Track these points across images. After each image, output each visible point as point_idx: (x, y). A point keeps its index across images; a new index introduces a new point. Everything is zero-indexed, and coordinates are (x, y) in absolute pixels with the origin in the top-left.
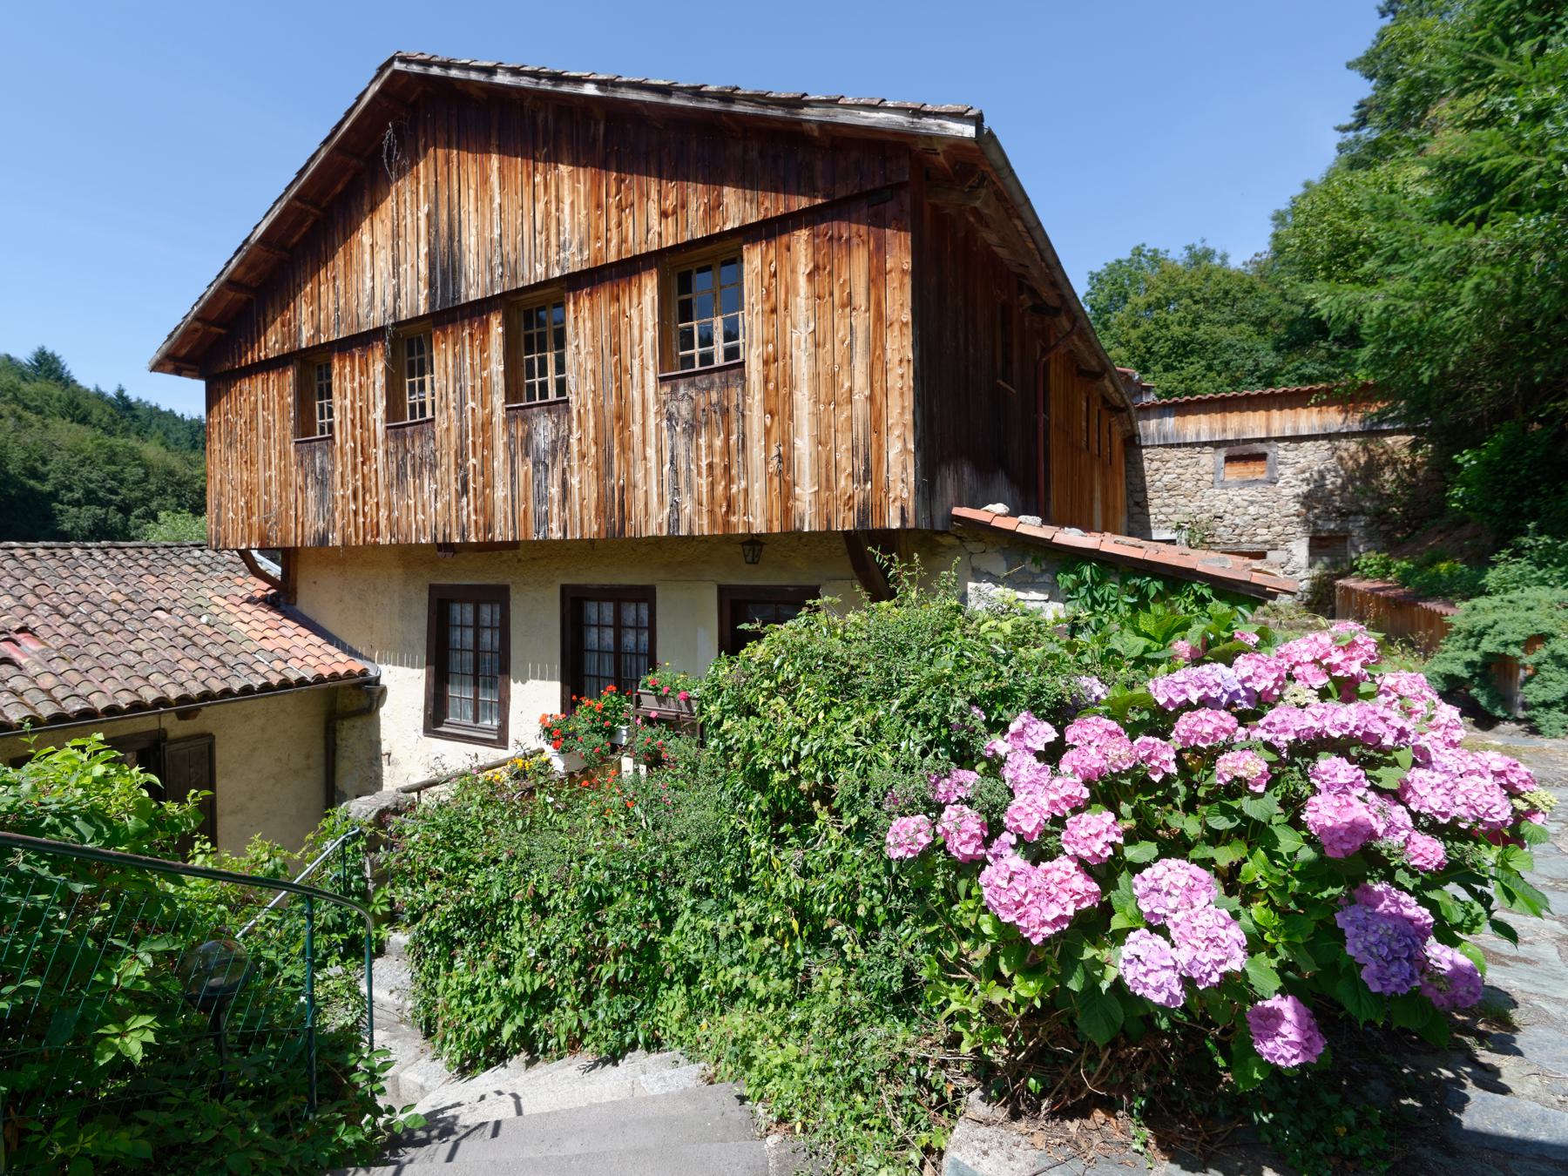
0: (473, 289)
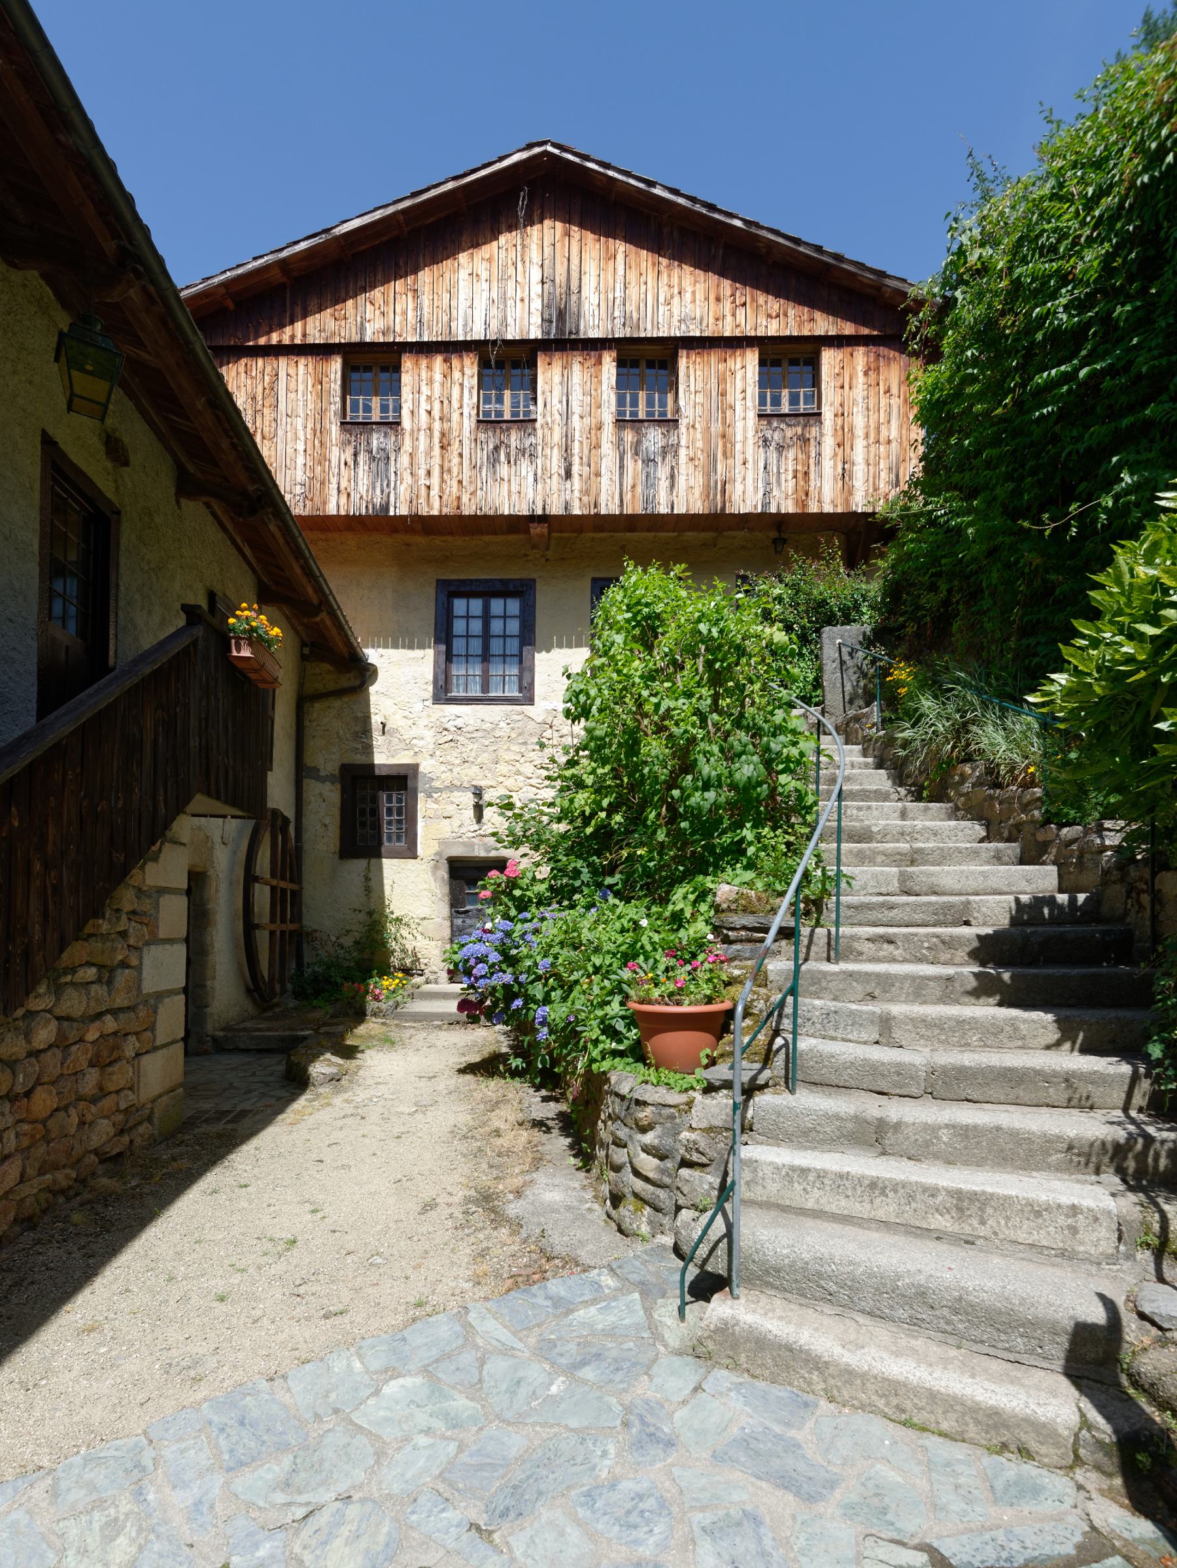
0: (593, 326)
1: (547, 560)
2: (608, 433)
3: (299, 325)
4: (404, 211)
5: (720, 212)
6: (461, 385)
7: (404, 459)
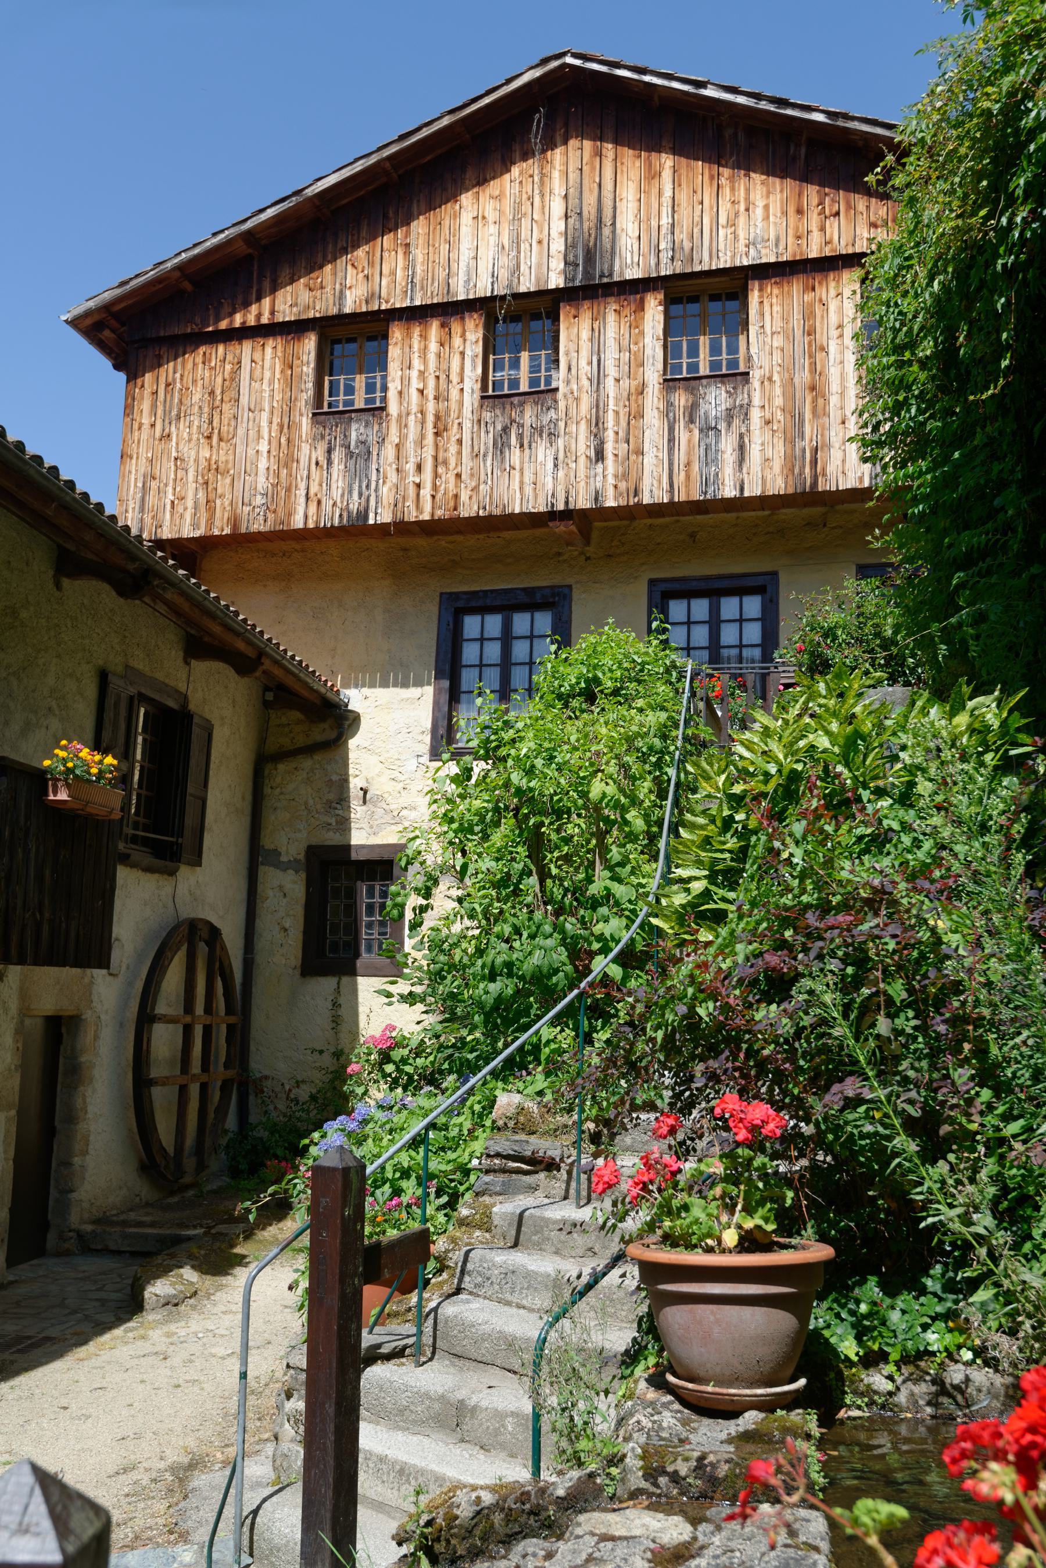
1: (588, 559)
2: (653, 399)
3: (266, 302)
4: (389, 158)
5: (794, 106)
6: (463, 354)
7: (389, 452)
